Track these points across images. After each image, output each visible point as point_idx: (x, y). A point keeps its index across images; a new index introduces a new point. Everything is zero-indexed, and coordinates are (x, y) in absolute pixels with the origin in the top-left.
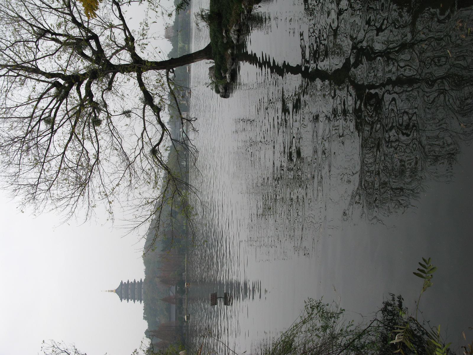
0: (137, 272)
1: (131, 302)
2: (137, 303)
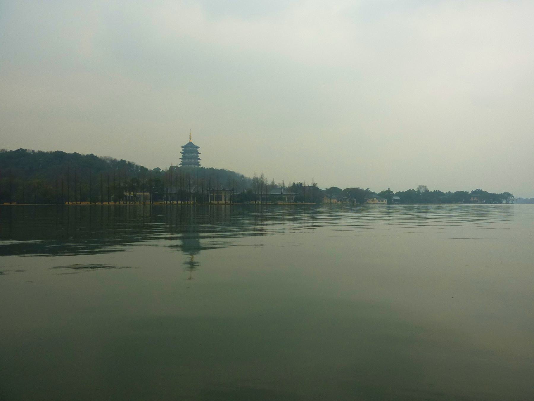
0: (207, 161)
1: (181, 156)
2: (180, 161)
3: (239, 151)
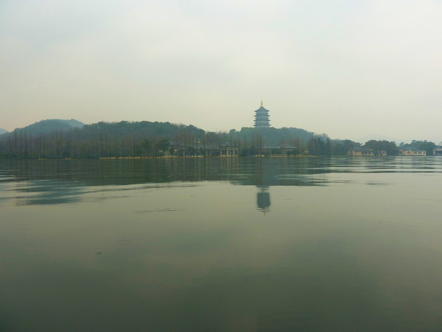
0: (276, 122)
1: (254, 118)
2: (254, 123)
3: (302, 110)
